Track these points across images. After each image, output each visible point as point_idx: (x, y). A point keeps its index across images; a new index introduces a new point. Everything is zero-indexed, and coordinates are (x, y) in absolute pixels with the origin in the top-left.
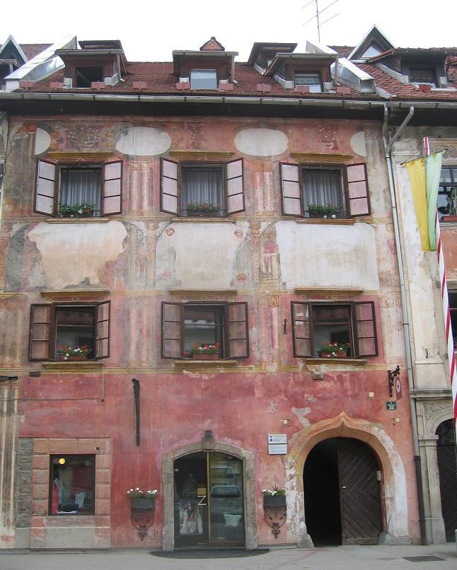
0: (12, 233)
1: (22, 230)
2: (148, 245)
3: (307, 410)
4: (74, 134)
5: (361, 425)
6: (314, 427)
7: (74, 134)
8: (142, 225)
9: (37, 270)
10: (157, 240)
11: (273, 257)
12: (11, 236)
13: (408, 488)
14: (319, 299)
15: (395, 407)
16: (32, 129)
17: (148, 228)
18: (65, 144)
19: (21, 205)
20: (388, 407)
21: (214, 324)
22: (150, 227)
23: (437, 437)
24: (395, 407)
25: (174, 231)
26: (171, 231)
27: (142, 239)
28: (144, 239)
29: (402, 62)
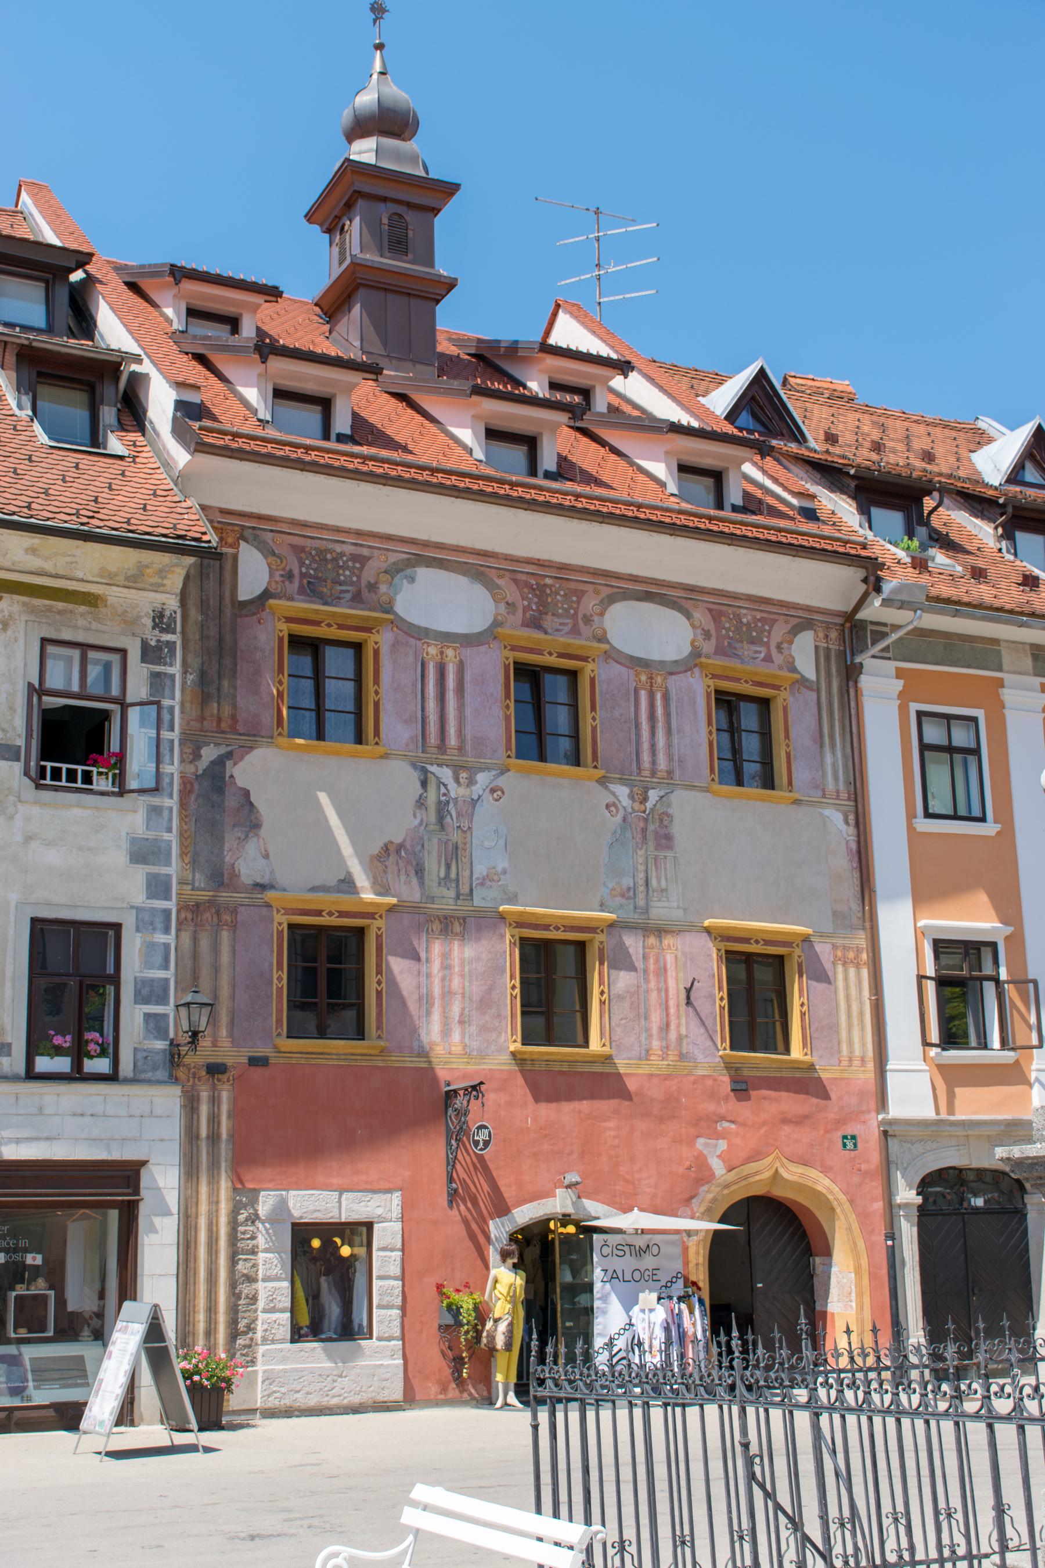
0: (203, 764)
1: (220, 763)
2: (459, 815)
3: (722, 1145)
4: (315, 566)
5: (792, 1173)
6: (732, 1176)
7: (315, 566)
8: (446, 774)
9: (252, 848)
10: (474, 807)
11: (538, 1394)
12: (200, 772)
13: (131, 763)
14: (968, 667)
15: (855, 1145)
16: (230, 540)
17: (457, 780)
18: (296, 584)
19: (215, 705)
20: (845, 1145)
21: (693, 1412)
22: (461, 780)
23: (919, 1200)
24: (855, 1145)
25: (503, 793)
26: (499, 793)
27: (448, 802)
28: (451, 805)
29: (856, 486)
